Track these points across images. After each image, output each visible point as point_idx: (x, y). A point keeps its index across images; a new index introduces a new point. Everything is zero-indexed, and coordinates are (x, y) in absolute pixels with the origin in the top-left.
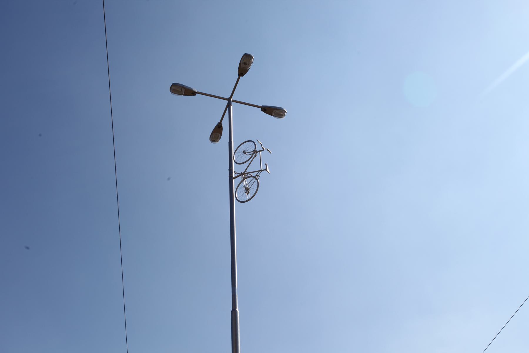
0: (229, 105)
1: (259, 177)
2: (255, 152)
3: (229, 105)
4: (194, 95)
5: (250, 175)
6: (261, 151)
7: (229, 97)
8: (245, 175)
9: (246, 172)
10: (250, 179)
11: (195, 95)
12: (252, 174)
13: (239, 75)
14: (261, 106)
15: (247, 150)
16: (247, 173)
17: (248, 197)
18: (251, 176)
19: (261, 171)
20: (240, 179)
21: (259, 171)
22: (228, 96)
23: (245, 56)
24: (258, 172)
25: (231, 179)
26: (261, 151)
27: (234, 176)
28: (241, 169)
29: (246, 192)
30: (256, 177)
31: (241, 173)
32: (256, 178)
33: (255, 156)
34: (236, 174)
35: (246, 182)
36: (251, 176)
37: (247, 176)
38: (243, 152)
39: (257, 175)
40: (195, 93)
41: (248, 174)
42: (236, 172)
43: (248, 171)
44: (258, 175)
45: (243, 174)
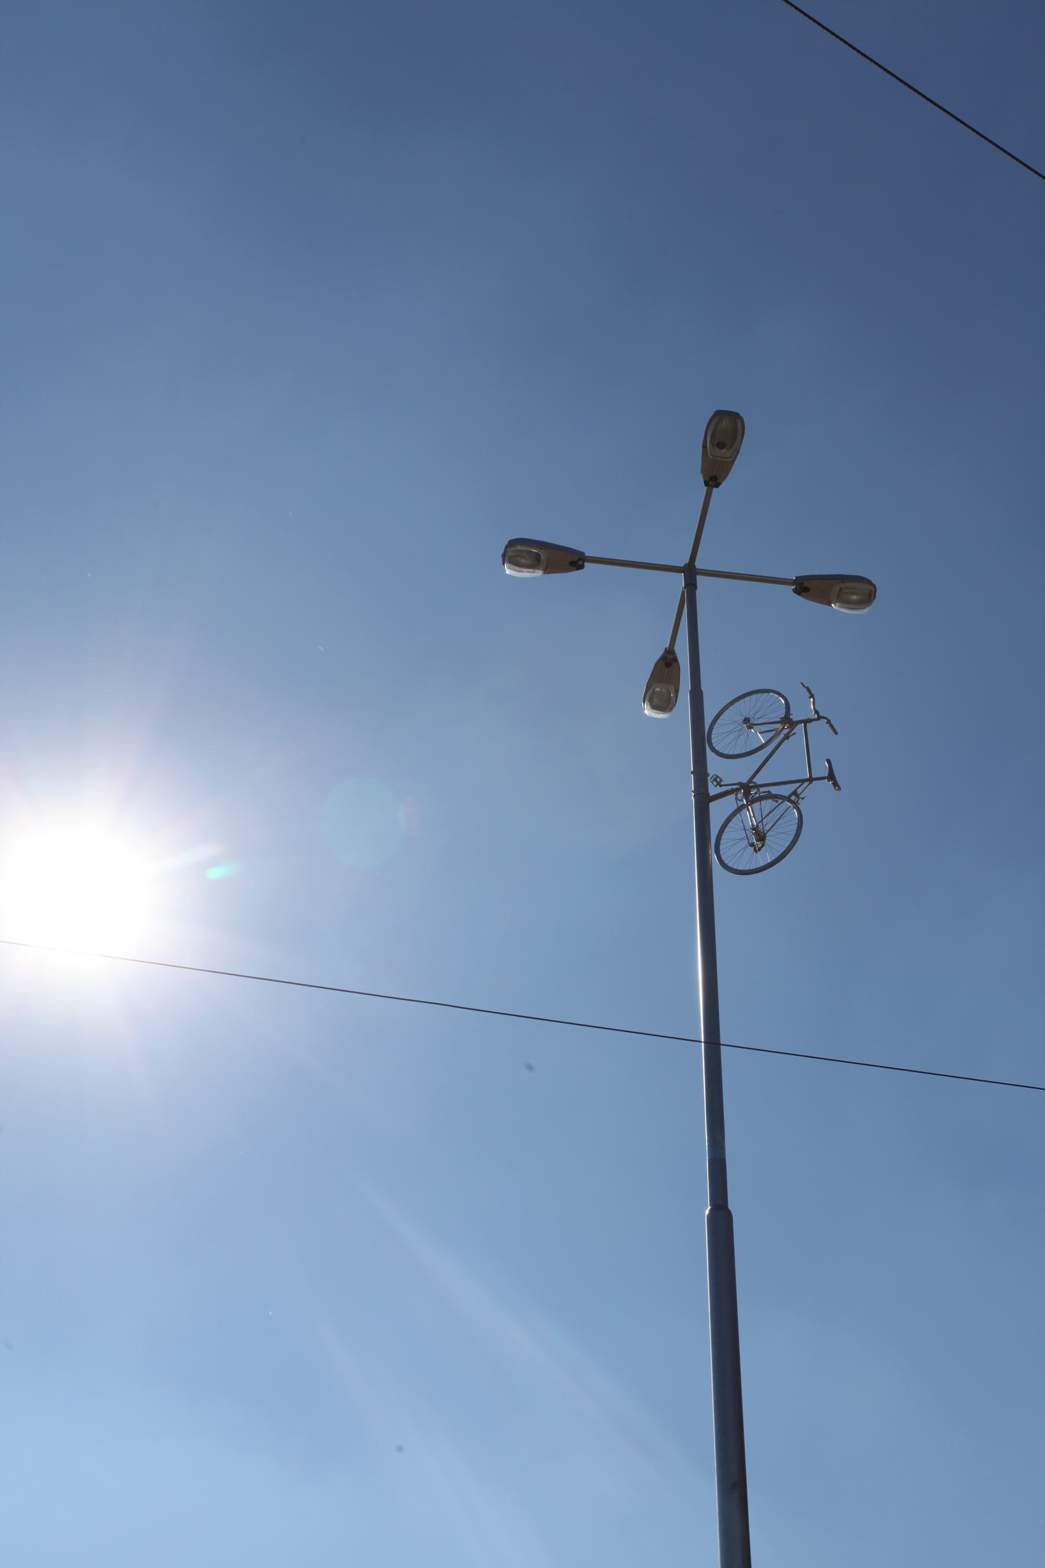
0: (691, 586)
1: (800, 800)
2: (787, 720)
3: (691, 586)
4: (578, 569)
5: (769, 791)
6: (810, 721)
7: (687, 561)
8: (758, 790)
9: (754, 783)
10: (768, 804)
11: (582, 567)
12: (774, 790)
13: (706, 483)
14: (704, 489)
15: (756, 716)
16: (758, 786)
17: (766, 856)
18: (770, 796)
19: (811, 780)
20: (729, 804)
21: (802, 781)
22: (683, 561)
23: (717, 418)
24: (799, 784)
25: (703, 802)
26: (810, 721)
27: (713, 790)
28: (734, 772)
29: (752, 845)
30: (793, 798)
31: (740, 784)
32: (794, 799)
33: (787, 737)
34: (721, 786)
35: (749, 817)
36: (770, 796)
37: (757, 795)
38: (746, 720)
39: (795, 793)
40: (581, 563)
41: (762, 789)
42: (721, 780)
43: (758, 780)
44: (799, 791)
45: (746, 788)
